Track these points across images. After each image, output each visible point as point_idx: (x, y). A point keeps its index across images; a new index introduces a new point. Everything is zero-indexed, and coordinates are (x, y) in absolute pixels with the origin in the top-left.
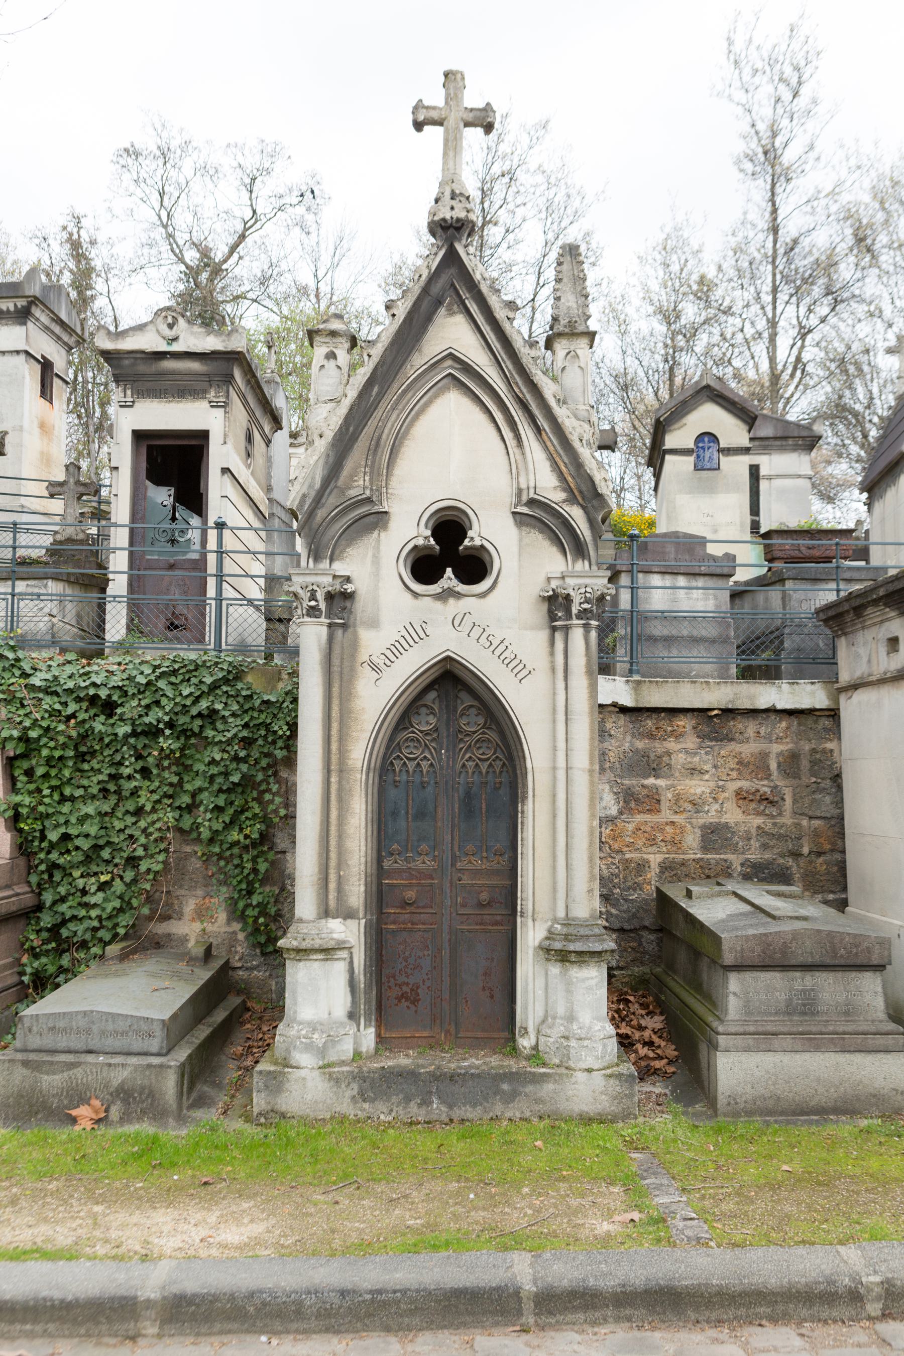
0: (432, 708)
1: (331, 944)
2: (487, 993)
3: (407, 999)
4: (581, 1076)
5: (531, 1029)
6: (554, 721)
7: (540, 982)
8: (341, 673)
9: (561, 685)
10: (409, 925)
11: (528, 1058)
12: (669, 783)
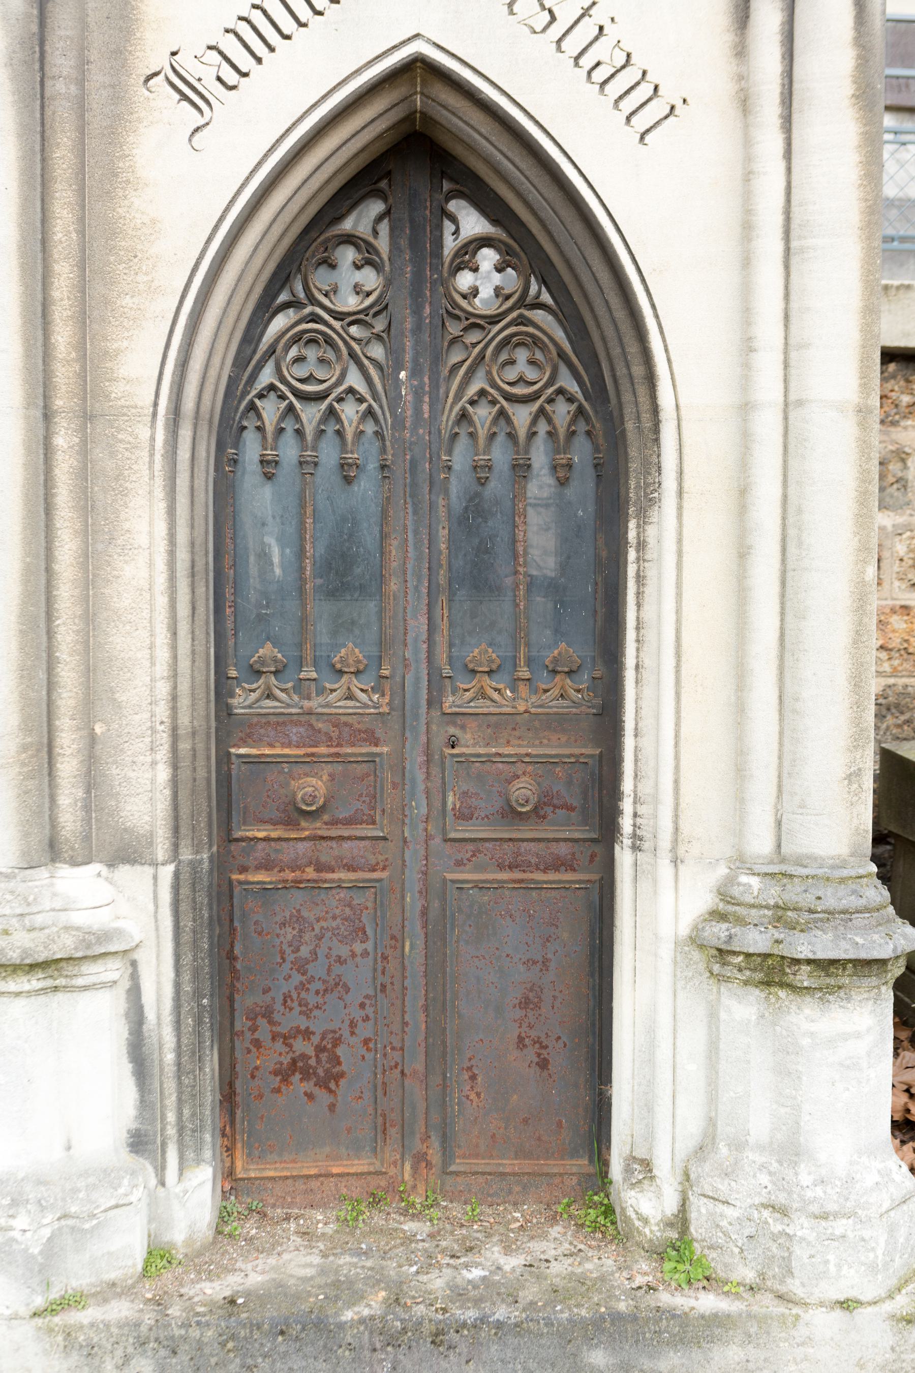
0: (370, 248)
1: (65, 946)
2: (531, 1054)
3: (307, 1074)
4: (823, 1323)
5: (664, 1167)
6: (746, 262)
7: (694, 1038)
8: (81, 106)
9: (770, 141)
10: (310, 873)
11: (658, 1253)
12: (900, 520)
